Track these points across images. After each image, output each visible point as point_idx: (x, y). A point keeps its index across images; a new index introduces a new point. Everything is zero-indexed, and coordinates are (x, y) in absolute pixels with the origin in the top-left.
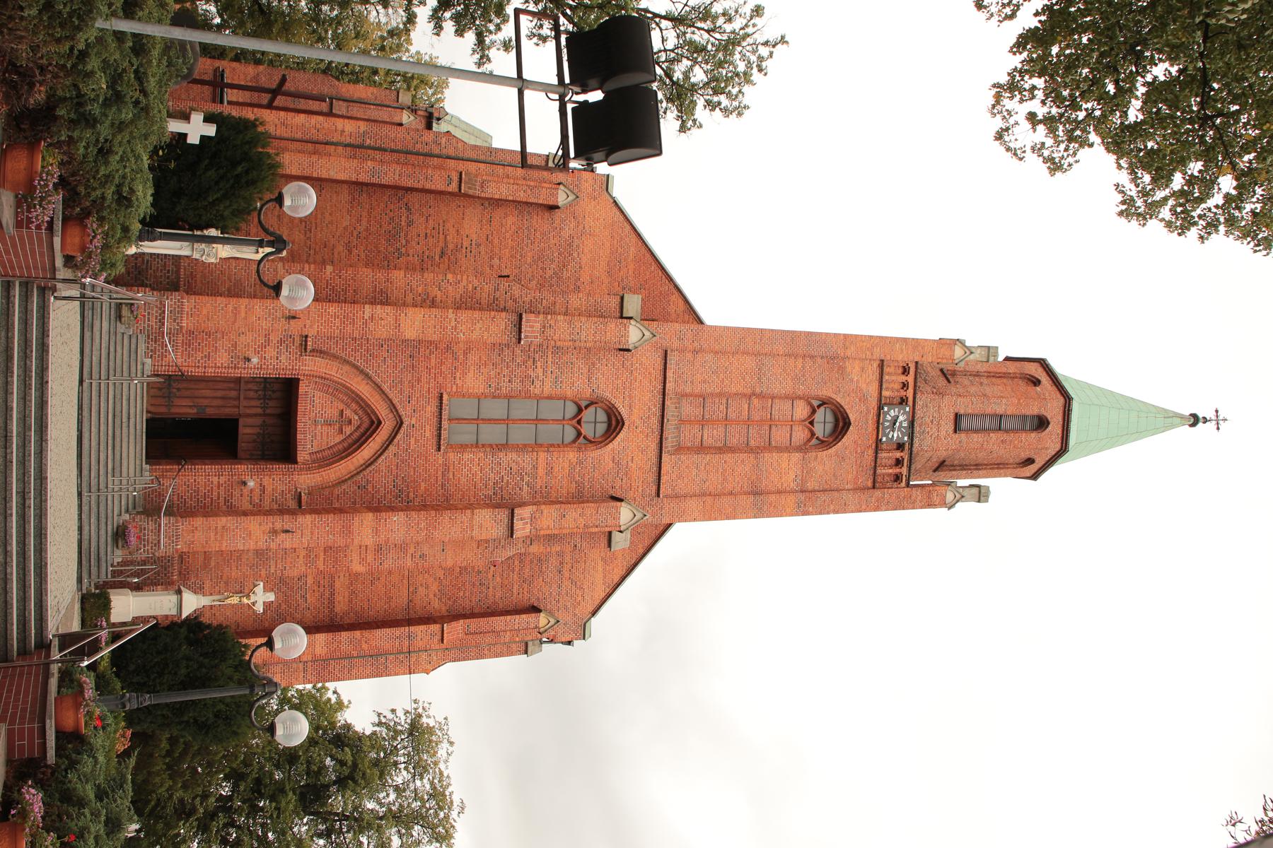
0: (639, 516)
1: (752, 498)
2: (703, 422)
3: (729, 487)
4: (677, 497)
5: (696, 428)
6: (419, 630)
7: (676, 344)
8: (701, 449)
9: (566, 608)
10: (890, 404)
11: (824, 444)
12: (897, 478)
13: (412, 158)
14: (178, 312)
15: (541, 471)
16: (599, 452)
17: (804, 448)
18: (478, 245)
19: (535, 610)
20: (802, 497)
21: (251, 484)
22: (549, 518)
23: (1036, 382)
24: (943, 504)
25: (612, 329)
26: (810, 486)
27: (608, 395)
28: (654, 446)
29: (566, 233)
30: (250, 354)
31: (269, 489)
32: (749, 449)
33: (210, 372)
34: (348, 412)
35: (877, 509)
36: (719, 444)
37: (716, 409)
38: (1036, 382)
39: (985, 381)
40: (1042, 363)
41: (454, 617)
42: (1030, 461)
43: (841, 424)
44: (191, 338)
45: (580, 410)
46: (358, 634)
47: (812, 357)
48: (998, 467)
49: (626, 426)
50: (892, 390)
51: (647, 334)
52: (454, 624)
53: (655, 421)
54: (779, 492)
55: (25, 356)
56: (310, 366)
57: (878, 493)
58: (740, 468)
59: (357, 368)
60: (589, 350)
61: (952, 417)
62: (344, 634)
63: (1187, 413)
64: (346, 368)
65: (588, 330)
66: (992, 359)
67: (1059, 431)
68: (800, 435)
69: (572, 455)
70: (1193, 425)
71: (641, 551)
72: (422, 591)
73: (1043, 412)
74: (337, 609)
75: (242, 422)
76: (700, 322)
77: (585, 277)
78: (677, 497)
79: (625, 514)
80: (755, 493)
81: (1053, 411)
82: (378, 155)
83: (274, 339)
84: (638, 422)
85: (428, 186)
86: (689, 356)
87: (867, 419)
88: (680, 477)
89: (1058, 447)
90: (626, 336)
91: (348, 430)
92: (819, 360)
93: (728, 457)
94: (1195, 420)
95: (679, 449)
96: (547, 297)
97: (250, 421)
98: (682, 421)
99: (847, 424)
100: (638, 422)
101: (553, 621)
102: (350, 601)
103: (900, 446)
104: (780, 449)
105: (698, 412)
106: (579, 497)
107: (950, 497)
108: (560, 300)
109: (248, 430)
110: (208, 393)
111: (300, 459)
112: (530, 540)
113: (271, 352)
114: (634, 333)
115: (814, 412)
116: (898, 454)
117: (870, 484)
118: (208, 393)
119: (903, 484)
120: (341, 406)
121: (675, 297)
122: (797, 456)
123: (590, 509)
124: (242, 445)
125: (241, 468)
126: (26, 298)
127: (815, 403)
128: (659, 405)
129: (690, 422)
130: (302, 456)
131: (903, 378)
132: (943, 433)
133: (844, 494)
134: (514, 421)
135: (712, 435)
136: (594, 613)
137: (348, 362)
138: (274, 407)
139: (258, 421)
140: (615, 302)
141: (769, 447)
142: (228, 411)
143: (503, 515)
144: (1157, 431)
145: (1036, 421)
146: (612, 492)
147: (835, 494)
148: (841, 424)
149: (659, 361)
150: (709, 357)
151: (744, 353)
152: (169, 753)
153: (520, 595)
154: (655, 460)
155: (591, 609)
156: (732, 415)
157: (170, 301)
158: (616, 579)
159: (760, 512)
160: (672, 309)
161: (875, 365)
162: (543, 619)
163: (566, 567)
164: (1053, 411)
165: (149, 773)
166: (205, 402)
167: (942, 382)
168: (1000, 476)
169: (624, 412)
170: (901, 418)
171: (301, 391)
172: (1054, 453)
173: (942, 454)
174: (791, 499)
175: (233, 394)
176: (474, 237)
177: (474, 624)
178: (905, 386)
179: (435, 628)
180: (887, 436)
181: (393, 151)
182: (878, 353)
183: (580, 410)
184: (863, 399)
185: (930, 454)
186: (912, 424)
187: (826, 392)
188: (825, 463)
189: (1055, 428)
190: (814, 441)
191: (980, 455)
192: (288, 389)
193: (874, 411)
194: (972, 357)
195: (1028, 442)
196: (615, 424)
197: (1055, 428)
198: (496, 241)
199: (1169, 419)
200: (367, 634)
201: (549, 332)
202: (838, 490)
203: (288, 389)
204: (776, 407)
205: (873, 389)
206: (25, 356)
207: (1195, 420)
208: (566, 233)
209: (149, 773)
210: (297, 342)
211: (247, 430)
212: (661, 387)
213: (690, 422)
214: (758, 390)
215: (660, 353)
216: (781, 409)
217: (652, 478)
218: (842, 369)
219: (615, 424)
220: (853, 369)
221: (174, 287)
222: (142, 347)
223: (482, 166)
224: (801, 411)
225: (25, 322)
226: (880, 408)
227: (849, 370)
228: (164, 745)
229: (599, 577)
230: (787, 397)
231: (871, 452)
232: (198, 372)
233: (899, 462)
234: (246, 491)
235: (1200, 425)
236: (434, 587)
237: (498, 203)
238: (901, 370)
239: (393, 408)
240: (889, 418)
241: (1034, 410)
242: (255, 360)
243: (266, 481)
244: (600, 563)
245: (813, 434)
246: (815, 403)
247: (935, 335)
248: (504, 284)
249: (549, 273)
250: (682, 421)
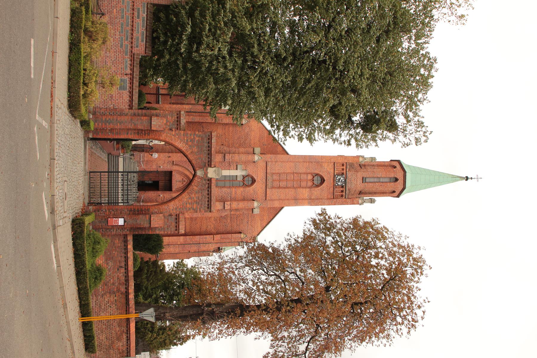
0: (259, 204)
1: (294, 201)
2: (280, 181)
3: (287, 198)
4: (272, 200)
5: (278, 182)
6: (208, 236)
7: (270, 160)
8: (279, 187)
9: (250, 233)
10: (338, 175)
11: (317, 186)
12: (342, 196)
13: (203, 114)
14: (144, 157)
15: (233, 193)
16: (249, 188)
17: (310, 187)
18: (222, 135)
19: (241, 233)
20: (310, 201)
21: (161, 196)
22: (235, 205)
23: (395, 167)
24: (358, 203)
25: (250, 157)
26: (313, 198)
27: (251, 174)
28: (264, 187)
29: (246, 131)
30: (160, 165)
31: (166, 197)
32: (294, 187)
33: (152, 170)
34: (184, 179)
35: (335, 204)
36: (285, 186)
37: (284, 177)
38: (395, 167)
39: (376, 167)
40: (399, 161)
41: (218, 233)
42: (394, 192)
43: (323, 181)
44: (147, 162)
45: (244, 178)
46: (191, 237)
47: (312, 162)
48: (383, 193)
49: (256, 182)
50: (339, 171)
51: (260, 158)
52: (217, 235)
53: (264, 180)
54: (303, 199)
55: (116, 166)
56: (174, 168)
57: (335, 200)
58: (291, 193)
59: (185, 168)
60: (245, 162)
61: (362, 178)
62: (188, 237)
63: (465, 176)
64: (183, 168)
65: (244, 157)
66: (373, 161)
67: (403, 182)
68: (310, 184)
69: (242, 189)
70: (467, 180)
71: (272, 218)
72: (209, 227)
73: (396, 176)
74: (187, 231)
75: (160, 182)
76: (288, 154)
77: (252, 142)
78: (272, 200)
79: (256, 204)
80: (295, 200)
81: (400, 176)
82: (194, 114)
83: (166, 162)
84: (260, 180)
85: (207, 121)
86: (274, 163)
87: (330, 180)
88: (272, 195)
89: (402, 187)
90: (254, 158)
91: (184, 183)
92: (314, 163)
93: (287, 190)
94: (467, 178)
95: (273, 187)
96: (233, 149)
97: (162, 181)
98: (273, 180)
99: (324, 180)
100: (260, 180)
101: (245, 236)
102: (190, 229)
103: (342, 187)
104: (303, 188)
105: (278, 178)
106: (244, 200)
107: (360, 201)
108: (237, 150)
109: (162, 184)
110: (152, 175)
111: (173, 190)
112: (231, 210)
113: (165, 165)
114: (256, 158)
115: (314, 177)
116: (342, 189)
117: (332, 197)
118: (152, 175)
119: (344, 197)
120: (183, 177)
121: (279, 147)
122: (308, 190)
123: (246, 203)
124: (160, 187)
125: (159, 192)
126: (116, 158)
127: (314, 175)
128: (265, 176)
129: (276, 180)
130: (173, 189)
131: (342, 167)
132: (358, 183)
133: (324, 200)
134: (226, 181)
135: (283, 184)
136: (258, 235)
137: (184, 167)
138: (167, 178)
139: (164, 181)
140: (252, 150)
141: (300, 187)
142: (156, 179)
143: (222, 204)
144: (449, 182)
145: (394, 179)
146: (253, 199)
147: (321, 200)
148: (323, 181)
149: (265, 164)
150: (279, 163)
151: (290, 162)
152: (147, 274)
153: (236, 228)
154: (265, 190)
155: (257, 234)
156: (288, 178)
157: (142, 154)
158: (264, 226)
159: (296, 204)
160: (278, 150)
161: (332, 164)
162: (242, 235)
163: (249, 222)
164: (400, 176)
165: (142, 279)
166: (151, 177)
167: (359, 168)
168: (384, 196)
169: (256, 178)
170: (342, 179)
171: (173, 174)
173: (360, 189)
174: (306, 201)
175: (158, 175)
176: (221, 133)
177: (223, 236)
178: (343, 169)
179: (212, 236)
180: (337, 184)
181: (198, 112)
182: (333, 160)
183: (244, 178)
184: (329, 173)
185: (355, 189)
186: (345, 180)
187: (316, 172)
188: (317, 192)
189: (401, 181)
190: (314, 185)
191: (373, 190)
192: (170, 174)
193: (332, 177)
194: (366, 160)
195: (391, 186)
196: (254, 181)
197: (401, 181)
198: (227, 134)
200: (194, 237)
201: (233, 158)
202: (321, 199)
203: (170, 174)
204: (302, 176)
205: (332, 171)
206: (116, 166)
207: (467, 178)
208: (246, 131)
209: (142, 279)
210: (172, 162)
211: (161, 184)
212: (265, 171)
213: (276, 180)
214: (295, 172)
215: (265, 162)
216: (304, 177)
217: (264, 195)
218: (321, 166)
219: (254, 181)
220: (325, 166)
221: (143, 151)
222: (136, 165)
223: (222, 115)
224: (310, 177)
225: (116, 161)
226: (334, 176)
227: (324, 165)
228: (146, 271)
229: (259, 225)
230: (304, 173)
231: (332, 188)
232: (149, 170)
233: (342, 191)
234: (160, 198)
235: (469, 180)
236: (212, 226)
237: (227, 124)
238: (341, 165)
240: (337, 179)
241: (392, 175)
242: (162, 167)
243: (165, 195)
244: (259, 222)
245: (314, 184)
246: (314, 175)
247: (355, 155)
248: (222, 147)
249: (242, 142)
250: (273, 180)
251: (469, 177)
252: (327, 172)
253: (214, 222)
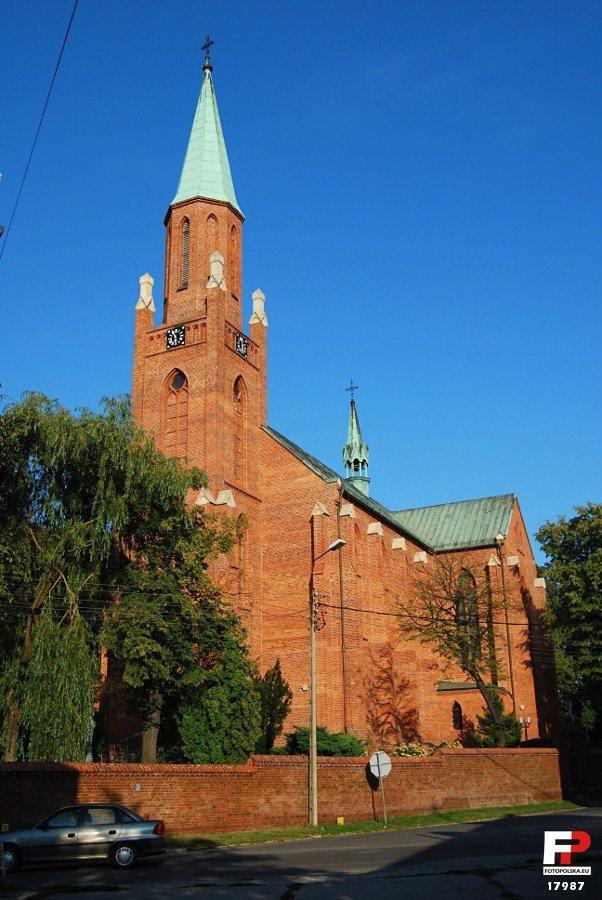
189: (215, 209)
253: (298, 577)
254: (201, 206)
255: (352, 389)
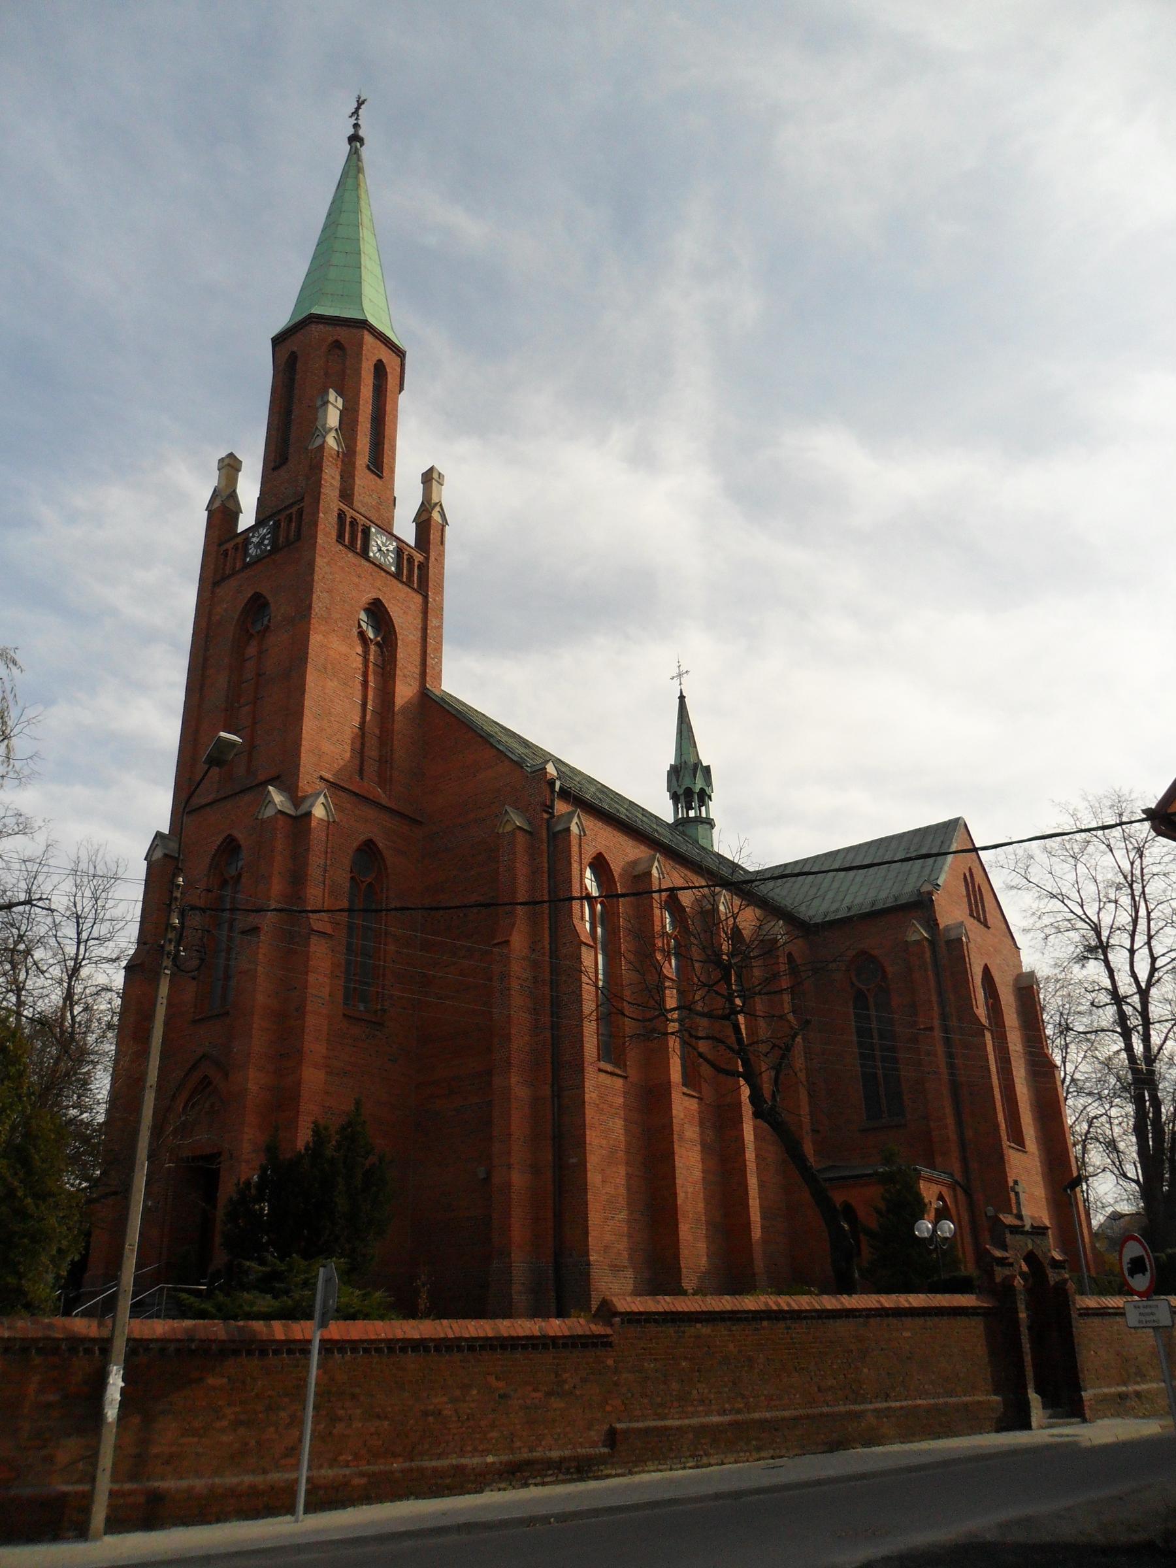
172: (321, 326)
199: (353, 167)
239: (194, 1067)
251: (351, 131)
252: (235, 597)
254: (316, 330)
255: (680, 675)
